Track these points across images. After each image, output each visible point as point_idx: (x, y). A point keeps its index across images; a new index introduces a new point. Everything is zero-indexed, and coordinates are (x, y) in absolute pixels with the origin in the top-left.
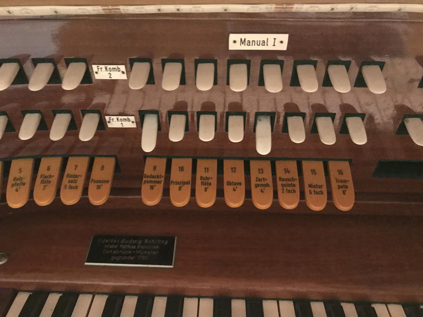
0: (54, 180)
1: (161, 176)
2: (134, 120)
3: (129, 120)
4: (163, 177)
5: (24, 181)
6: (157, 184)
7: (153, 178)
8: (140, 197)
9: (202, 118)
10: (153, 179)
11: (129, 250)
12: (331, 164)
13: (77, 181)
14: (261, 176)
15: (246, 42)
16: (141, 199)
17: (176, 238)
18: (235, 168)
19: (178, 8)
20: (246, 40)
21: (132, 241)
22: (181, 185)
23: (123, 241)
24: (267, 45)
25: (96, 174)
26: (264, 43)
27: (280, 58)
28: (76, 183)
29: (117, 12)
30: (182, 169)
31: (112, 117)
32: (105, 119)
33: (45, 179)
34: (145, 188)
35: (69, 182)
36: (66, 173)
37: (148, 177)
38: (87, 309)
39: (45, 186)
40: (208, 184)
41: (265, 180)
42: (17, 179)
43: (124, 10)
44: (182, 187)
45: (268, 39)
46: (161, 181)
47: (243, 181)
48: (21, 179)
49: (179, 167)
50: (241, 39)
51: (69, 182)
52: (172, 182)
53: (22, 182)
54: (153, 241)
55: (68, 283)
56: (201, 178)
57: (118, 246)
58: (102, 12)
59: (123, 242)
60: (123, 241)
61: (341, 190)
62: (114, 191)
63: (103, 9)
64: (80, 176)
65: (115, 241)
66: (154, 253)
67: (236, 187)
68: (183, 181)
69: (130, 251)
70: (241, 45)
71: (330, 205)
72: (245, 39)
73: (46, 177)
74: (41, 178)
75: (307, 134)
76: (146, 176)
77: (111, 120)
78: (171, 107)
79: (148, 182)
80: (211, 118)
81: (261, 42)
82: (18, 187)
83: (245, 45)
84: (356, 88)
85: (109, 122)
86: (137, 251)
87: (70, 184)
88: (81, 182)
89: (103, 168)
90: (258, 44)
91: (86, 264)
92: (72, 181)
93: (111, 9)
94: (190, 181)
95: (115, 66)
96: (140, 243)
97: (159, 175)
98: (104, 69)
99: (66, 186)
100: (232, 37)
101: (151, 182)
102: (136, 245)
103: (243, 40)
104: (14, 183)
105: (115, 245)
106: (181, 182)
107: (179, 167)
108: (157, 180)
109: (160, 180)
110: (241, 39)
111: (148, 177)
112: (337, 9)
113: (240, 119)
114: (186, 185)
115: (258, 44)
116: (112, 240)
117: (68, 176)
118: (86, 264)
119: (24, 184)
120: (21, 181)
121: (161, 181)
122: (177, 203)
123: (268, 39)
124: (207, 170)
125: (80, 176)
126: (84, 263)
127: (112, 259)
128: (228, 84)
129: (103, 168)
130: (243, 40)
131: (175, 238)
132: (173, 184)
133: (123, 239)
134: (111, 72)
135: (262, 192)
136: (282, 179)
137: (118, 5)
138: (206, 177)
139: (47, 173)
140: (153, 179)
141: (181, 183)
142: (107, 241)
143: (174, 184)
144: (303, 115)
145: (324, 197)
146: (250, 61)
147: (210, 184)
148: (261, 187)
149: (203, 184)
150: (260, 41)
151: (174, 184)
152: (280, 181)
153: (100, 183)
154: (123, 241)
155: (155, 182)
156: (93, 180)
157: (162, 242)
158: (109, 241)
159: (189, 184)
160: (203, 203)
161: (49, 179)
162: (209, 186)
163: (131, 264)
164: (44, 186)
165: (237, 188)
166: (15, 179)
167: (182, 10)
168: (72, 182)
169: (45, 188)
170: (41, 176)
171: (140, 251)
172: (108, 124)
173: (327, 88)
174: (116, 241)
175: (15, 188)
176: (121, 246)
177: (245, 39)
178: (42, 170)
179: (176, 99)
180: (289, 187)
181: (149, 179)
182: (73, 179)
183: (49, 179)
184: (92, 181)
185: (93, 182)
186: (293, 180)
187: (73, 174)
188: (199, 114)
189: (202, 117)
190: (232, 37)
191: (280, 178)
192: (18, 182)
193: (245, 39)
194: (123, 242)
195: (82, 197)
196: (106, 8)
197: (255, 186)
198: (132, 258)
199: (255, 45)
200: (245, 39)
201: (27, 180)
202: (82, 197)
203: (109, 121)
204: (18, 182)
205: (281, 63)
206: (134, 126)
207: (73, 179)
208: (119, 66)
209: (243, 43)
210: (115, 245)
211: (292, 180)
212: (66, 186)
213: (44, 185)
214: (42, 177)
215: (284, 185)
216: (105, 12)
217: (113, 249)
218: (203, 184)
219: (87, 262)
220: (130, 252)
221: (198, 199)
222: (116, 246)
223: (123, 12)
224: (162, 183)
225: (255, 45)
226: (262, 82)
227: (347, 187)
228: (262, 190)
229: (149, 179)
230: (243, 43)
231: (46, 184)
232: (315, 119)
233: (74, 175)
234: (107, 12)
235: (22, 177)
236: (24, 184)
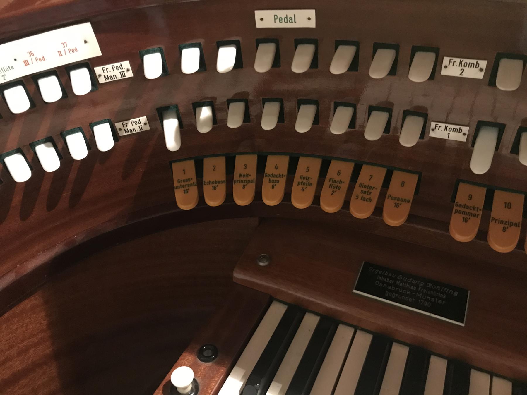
0: (345, 187)
1: (478, 208)
2: (467, 132)
3: (460, 131)
4: (480, 210)
5: (311, 181)
6: (472, 218)
7: (468, 209)
10: (465, 210)
11: (408, 290)
13: (371, 193)
15: (109, 78)
17: (469, 291)
20: (109, 76)
21: (412, 280)
22: (506, 226)
23: (400, 277)
24: (295, 22)
25: (394, 189)
28: (369, 195)
30: (508, 205)
31: (440, 124)
33: (333, 183)
34: (456, 220)
35: (362, 192)
36: (359, 181)
37: (460, 206)
38: (352, 346)
39: (334, 192)
42: (304, 178)
44: (507, 228)
45: (294, 15)
46: (478, 215)
48: (308, 178)
49: (505, 203)
51: (362, 192)
52: (493, 219)
53: (309, 182)
54: (438, 287)
55: (331, 309)
57: (393, 281)
59: (400, 278)
60: (401, 277)
62: (411, 218)
64: (375, 188)
65: (390, 275)
66: (440, 302)
68: (510, 221)
69: (409, 291)
73: (335, 182)
74: (329, 182)
76: (459, 204)
77: (437, 128)
79: (460, 212)
82: (305, 186)
85: (433, 130)
86: (417, 293)
87: (363, 194)
88: (375, 195)
89: (403, 184)
91: (354, 291)
92: (365, 192)
94: (521, 224)
95: (458, 127)
96: (422, 285)
98: (458, 63)
99: (357, 196)
101: (464, 213)
102: (417, 286)
103: (106, 76)
104: (301, 181)
105: (390, 279)
106: (506, 222)
107: (505, 203)
108: (473, 212)
109: (477, 213)
111: (460, 206)
114: (513, 227)
116: (387, 273)
117: (361, 185)
118: (354, 291)
119: (311, 185)
120: (308, 181)
121: (478, 215)
122: (497, 246)
123: (294, 15)
125: (375, 188)
126: (353, 290)
127: (387, 295)
129: (403, 184)
130: (106, 76)
131: (468, 291)
132: (494, 221)
133: (401, 275)
134: (465, 69)
139: (337, 178)
140: (465, 210)
141: (505, 223)
142: (380, 272)
143: (496, 222)
151: (496, 222)
153: (398, 201)
154: (401, 277)
155: (470, 214)
156: (390, 196)
157: (449, 292)
158: (383, 273)
159: (519, 227)
161: (339, 185)
162: (337, 190)
163: (410, 306)
164: (333, 191)
166: (301, 177)
168: (364, 192)
169: (333, 193)
170: (330, 180)
171: (421, 294)
172: (431, 132)
174: (392, 275)
175: (301, 186)
176: (398, 282)
178: (332, 173)
181: (462, 209)
182: (366, 190)
183: (339, 185)
184: (389, 197)
185: (390, 198)
187: (367, 185)
192: (305, 181)
194: (400, 278)
198: (410, 300)
201: (314, 180)
203: (434, 129)
204: (305, 181)
206: (464, 139)
207: (366, 190)
208: (480, 62)
210: (390, 279)
212: (357, 196)
213: (333, 190)
214: (331, 181)
217: (388, 284)
219: (355, 289)
220: (408, 293)
222: (391, 281)
224: (480, 217)
225: (473, 67)
229: (462, 209)
230: (107, 79)
231: (335, 190)
233: (368, 186)
235: (310, 177)
236: (311, 185)
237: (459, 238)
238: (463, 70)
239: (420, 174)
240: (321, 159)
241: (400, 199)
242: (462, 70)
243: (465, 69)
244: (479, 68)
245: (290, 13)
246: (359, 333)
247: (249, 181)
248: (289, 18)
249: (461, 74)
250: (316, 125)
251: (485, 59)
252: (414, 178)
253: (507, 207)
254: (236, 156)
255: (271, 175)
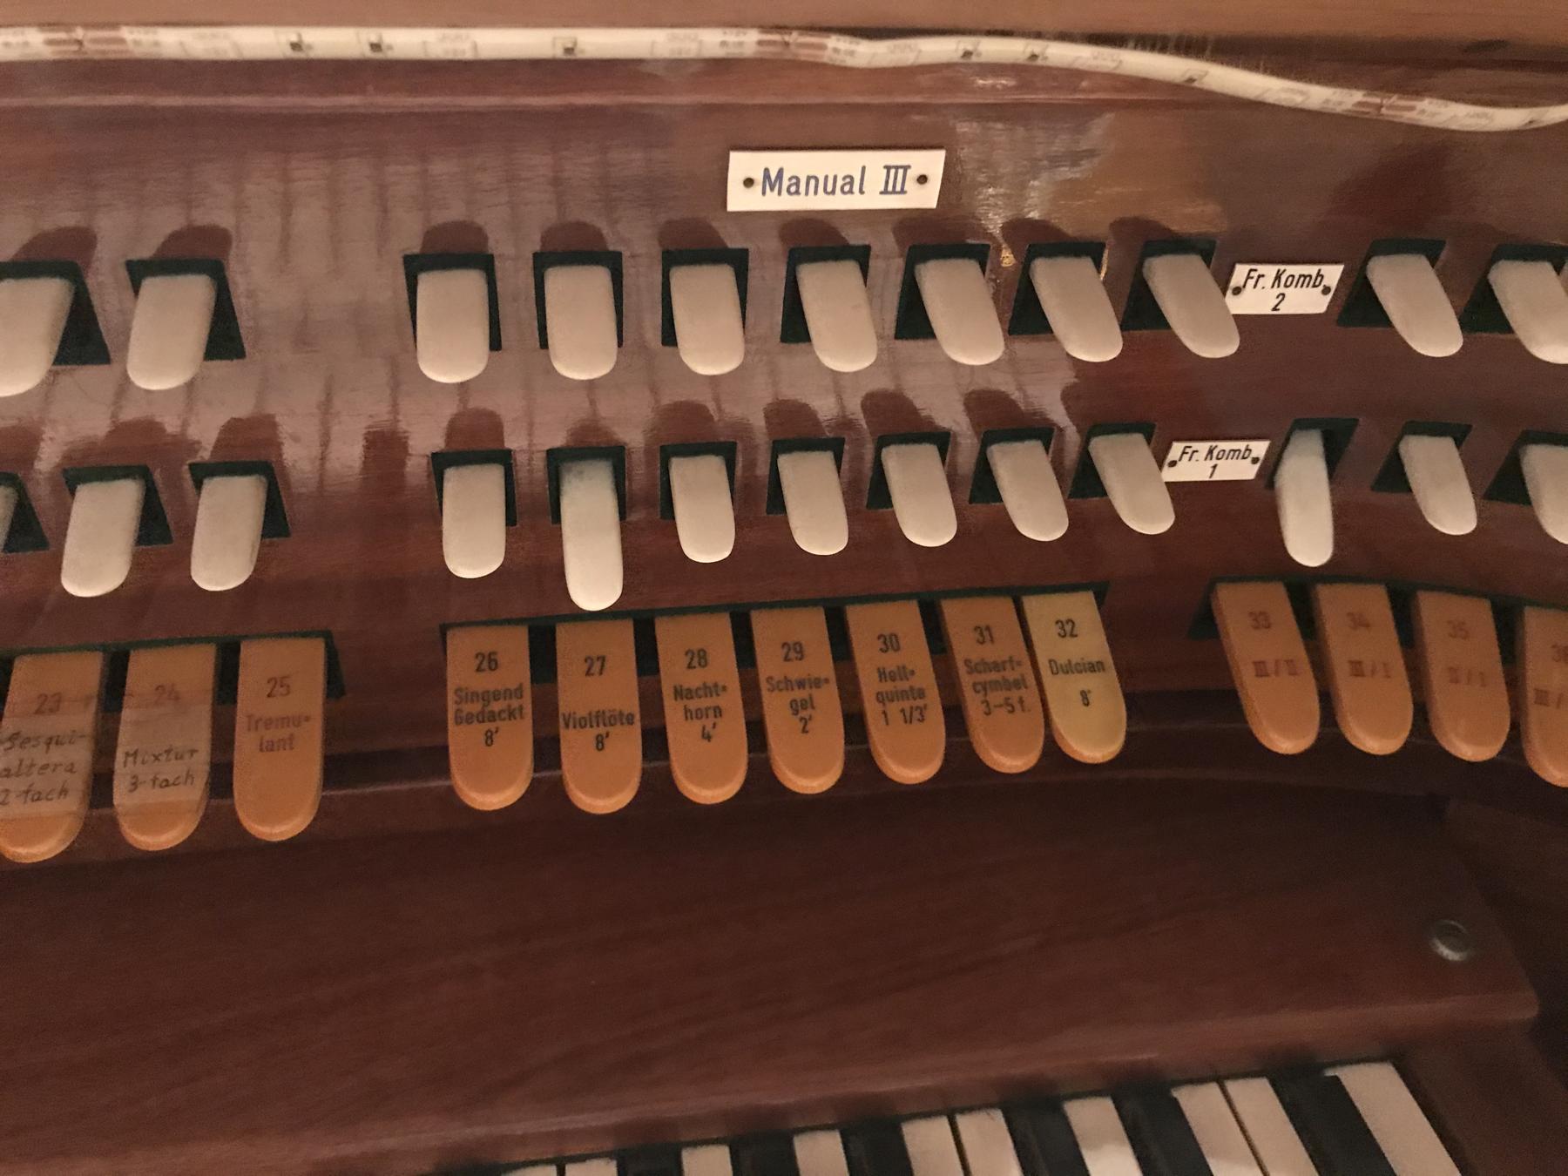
1: (716, 685)
8: (447, 783)
9: (454, 479)
12: (953, 611)
14: (891, 661)
15: (785, 183)
16: (451, 791)
18: (1070, 624)
19: (374, 39)
24: (861, 192)
26: (851, 183)
27: (855, 237)
29: (112, 51)
32: (1268, 452)
40: (915, 695)
41: (1015, 664)
43: (137, 43)
45: (864, 169)
47: (632, 705)
50: (767, 170)
56: (679, 693)
58: (48, 53)
61: (697, 726)
63: (50, 42)
67: (711, 726)
70: (764, 193)
71: (761, 773)
72: (780, 172)
75: (852, 515)
78: (438, 443)
80: (490, 480)
81: (840, 183)
83: (780, 193)
84: (899, 343)
90: (829, 189)
93: (93, 42)
97: (710, 684)
100: (742, 164)
103: (773, 176)
110: (767, 170)
112: (1046, 58)
113: (490, 480)
115: (829, 189)
117: (255, 723)
123: (864, 169)
124: (597, 665)
128: (669, 336)
130: (773, 176)
135: (707, 741)
136: (684, 693)
137: (115, 25)
138: (705, 686)
144: (942, 440)
145: (935, 731)
146: (744, 253)
147: (718, 712)
148: (901, 702)
149: (604, 720)
150: (835, 178)
152: (676, 699)
160: (584, 791)
165: (714, 725)
167: (390, 47)
173: (909, 347)
177: (781, 172)
179: (114, 416)
180: (903, 700)
182: (283, 733)
186: (787, 685)
188: (201, 473)
189: (452, 477)
190: (742, 164)
191: (967, 662)
193: (780, 172)
195: (537, 775)
196: (62, 35)
197: (792, 707)
199: (816, 192)
200: (781, 172)
202: (537, 775)
205: (861, 256)
207: (283, 733)
209: (772, 189)
211: (981, 668)
215: (884, 694)
216: (60, 52)
218: (604, 720)
221: (881, 750)
223: (139, 52)
225: (816, 192)
226: (795, 328)
227: (718, 712)
228: (707, 729)
230: (772, 189)
232: (985, 450)
234: (69, 52)
237: (1286, 745)
238: (1283, 295)
239: (327, 636)
240: (822, 610)
241: (291, 724)
242: (1281, 297)
243: (1287, 291)
244: (1321, 288)
245: (796, 163)
246: (963, 1121)
247: (481, 719)
248: (790, 179)
249: (1275, 309)
250: (1079, 500)
251: (1336, 262)
252: (313, 653)
253: (883, 680)
254: (132, 652)
255: (516, 690)
